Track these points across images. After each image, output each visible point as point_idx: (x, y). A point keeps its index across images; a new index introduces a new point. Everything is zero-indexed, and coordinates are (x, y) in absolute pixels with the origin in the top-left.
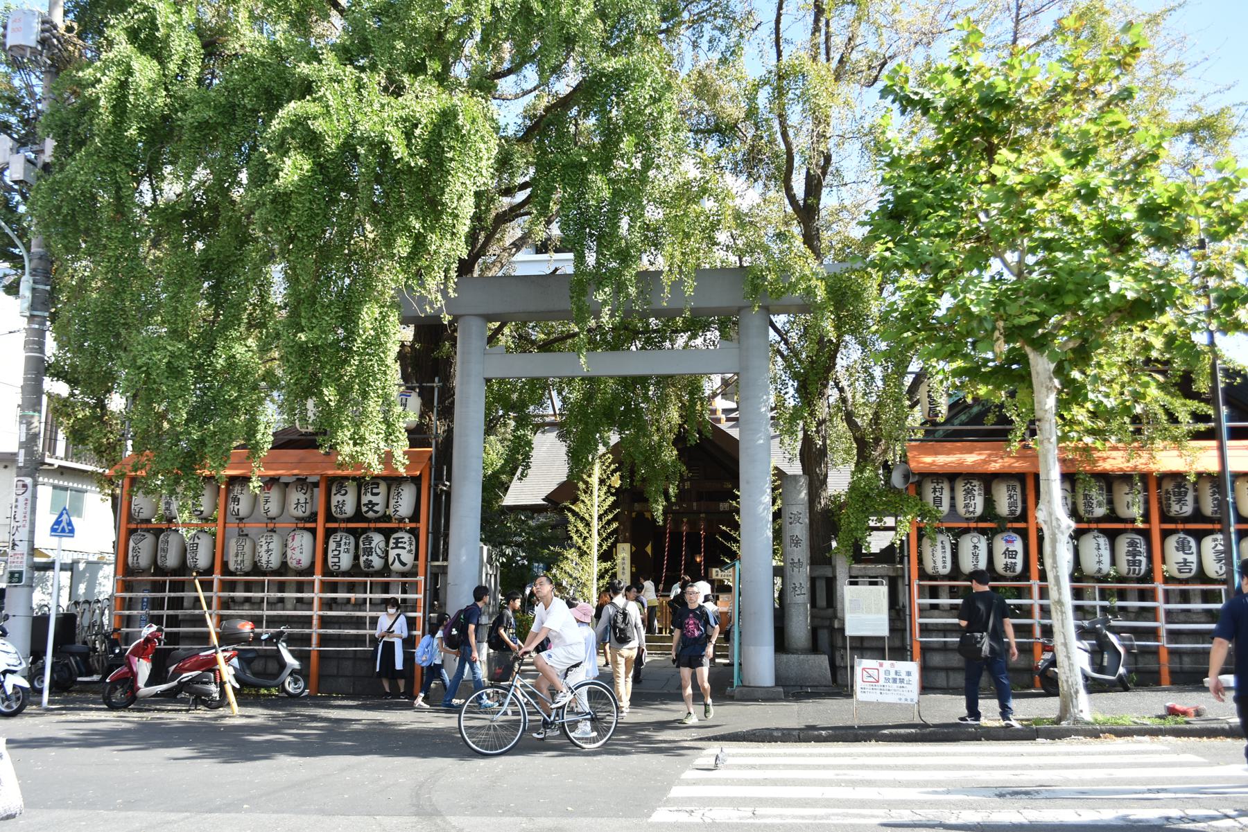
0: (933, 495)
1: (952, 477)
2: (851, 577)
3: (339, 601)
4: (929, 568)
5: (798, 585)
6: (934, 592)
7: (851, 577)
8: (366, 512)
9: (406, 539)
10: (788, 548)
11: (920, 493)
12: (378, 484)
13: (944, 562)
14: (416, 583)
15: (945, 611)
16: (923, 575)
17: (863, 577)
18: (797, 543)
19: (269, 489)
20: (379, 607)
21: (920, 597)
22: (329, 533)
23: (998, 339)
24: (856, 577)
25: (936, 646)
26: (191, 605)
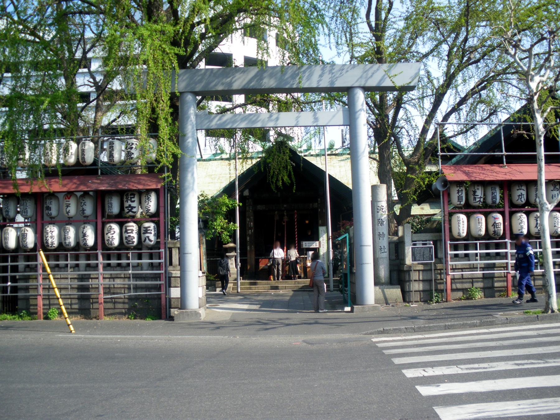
0: (458, 195)
1: (484, 184)
2: (413, 241)
3: (91, 265)
4: (455, 234)
5: (382, 247)
6: (455, 247)
7: (413, 241)
8: (128, 212)
9: (152, 228)
10: (377, 226)
11: (449, 195)
12: (134, 195)
13: (463, 230)
14: (160, 253)
15: (462, 258)
16: (452, 239)
17: (419, 241)
18: (251, 228)
19: (69, 199)
20: (115, 269)
21: (451, 251)
22: (512, 214)
23: (237, 29)
24: (416, 241)
25: (467, 270)
26: (23, 270)
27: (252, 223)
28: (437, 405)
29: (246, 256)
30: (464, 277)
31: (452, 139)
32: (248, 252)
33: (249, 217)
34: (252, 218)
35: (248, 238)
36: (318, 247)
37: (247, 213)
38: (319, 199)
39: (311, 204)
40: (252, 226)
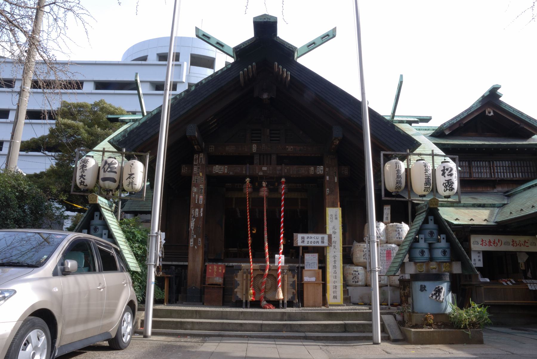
18: (198, 206)
27: (201, 197)
33: (197, 186)
34: (202, 186)
36: (326, 244)
37: (194, 178)
39: (312, 168)
40: (201, 202)
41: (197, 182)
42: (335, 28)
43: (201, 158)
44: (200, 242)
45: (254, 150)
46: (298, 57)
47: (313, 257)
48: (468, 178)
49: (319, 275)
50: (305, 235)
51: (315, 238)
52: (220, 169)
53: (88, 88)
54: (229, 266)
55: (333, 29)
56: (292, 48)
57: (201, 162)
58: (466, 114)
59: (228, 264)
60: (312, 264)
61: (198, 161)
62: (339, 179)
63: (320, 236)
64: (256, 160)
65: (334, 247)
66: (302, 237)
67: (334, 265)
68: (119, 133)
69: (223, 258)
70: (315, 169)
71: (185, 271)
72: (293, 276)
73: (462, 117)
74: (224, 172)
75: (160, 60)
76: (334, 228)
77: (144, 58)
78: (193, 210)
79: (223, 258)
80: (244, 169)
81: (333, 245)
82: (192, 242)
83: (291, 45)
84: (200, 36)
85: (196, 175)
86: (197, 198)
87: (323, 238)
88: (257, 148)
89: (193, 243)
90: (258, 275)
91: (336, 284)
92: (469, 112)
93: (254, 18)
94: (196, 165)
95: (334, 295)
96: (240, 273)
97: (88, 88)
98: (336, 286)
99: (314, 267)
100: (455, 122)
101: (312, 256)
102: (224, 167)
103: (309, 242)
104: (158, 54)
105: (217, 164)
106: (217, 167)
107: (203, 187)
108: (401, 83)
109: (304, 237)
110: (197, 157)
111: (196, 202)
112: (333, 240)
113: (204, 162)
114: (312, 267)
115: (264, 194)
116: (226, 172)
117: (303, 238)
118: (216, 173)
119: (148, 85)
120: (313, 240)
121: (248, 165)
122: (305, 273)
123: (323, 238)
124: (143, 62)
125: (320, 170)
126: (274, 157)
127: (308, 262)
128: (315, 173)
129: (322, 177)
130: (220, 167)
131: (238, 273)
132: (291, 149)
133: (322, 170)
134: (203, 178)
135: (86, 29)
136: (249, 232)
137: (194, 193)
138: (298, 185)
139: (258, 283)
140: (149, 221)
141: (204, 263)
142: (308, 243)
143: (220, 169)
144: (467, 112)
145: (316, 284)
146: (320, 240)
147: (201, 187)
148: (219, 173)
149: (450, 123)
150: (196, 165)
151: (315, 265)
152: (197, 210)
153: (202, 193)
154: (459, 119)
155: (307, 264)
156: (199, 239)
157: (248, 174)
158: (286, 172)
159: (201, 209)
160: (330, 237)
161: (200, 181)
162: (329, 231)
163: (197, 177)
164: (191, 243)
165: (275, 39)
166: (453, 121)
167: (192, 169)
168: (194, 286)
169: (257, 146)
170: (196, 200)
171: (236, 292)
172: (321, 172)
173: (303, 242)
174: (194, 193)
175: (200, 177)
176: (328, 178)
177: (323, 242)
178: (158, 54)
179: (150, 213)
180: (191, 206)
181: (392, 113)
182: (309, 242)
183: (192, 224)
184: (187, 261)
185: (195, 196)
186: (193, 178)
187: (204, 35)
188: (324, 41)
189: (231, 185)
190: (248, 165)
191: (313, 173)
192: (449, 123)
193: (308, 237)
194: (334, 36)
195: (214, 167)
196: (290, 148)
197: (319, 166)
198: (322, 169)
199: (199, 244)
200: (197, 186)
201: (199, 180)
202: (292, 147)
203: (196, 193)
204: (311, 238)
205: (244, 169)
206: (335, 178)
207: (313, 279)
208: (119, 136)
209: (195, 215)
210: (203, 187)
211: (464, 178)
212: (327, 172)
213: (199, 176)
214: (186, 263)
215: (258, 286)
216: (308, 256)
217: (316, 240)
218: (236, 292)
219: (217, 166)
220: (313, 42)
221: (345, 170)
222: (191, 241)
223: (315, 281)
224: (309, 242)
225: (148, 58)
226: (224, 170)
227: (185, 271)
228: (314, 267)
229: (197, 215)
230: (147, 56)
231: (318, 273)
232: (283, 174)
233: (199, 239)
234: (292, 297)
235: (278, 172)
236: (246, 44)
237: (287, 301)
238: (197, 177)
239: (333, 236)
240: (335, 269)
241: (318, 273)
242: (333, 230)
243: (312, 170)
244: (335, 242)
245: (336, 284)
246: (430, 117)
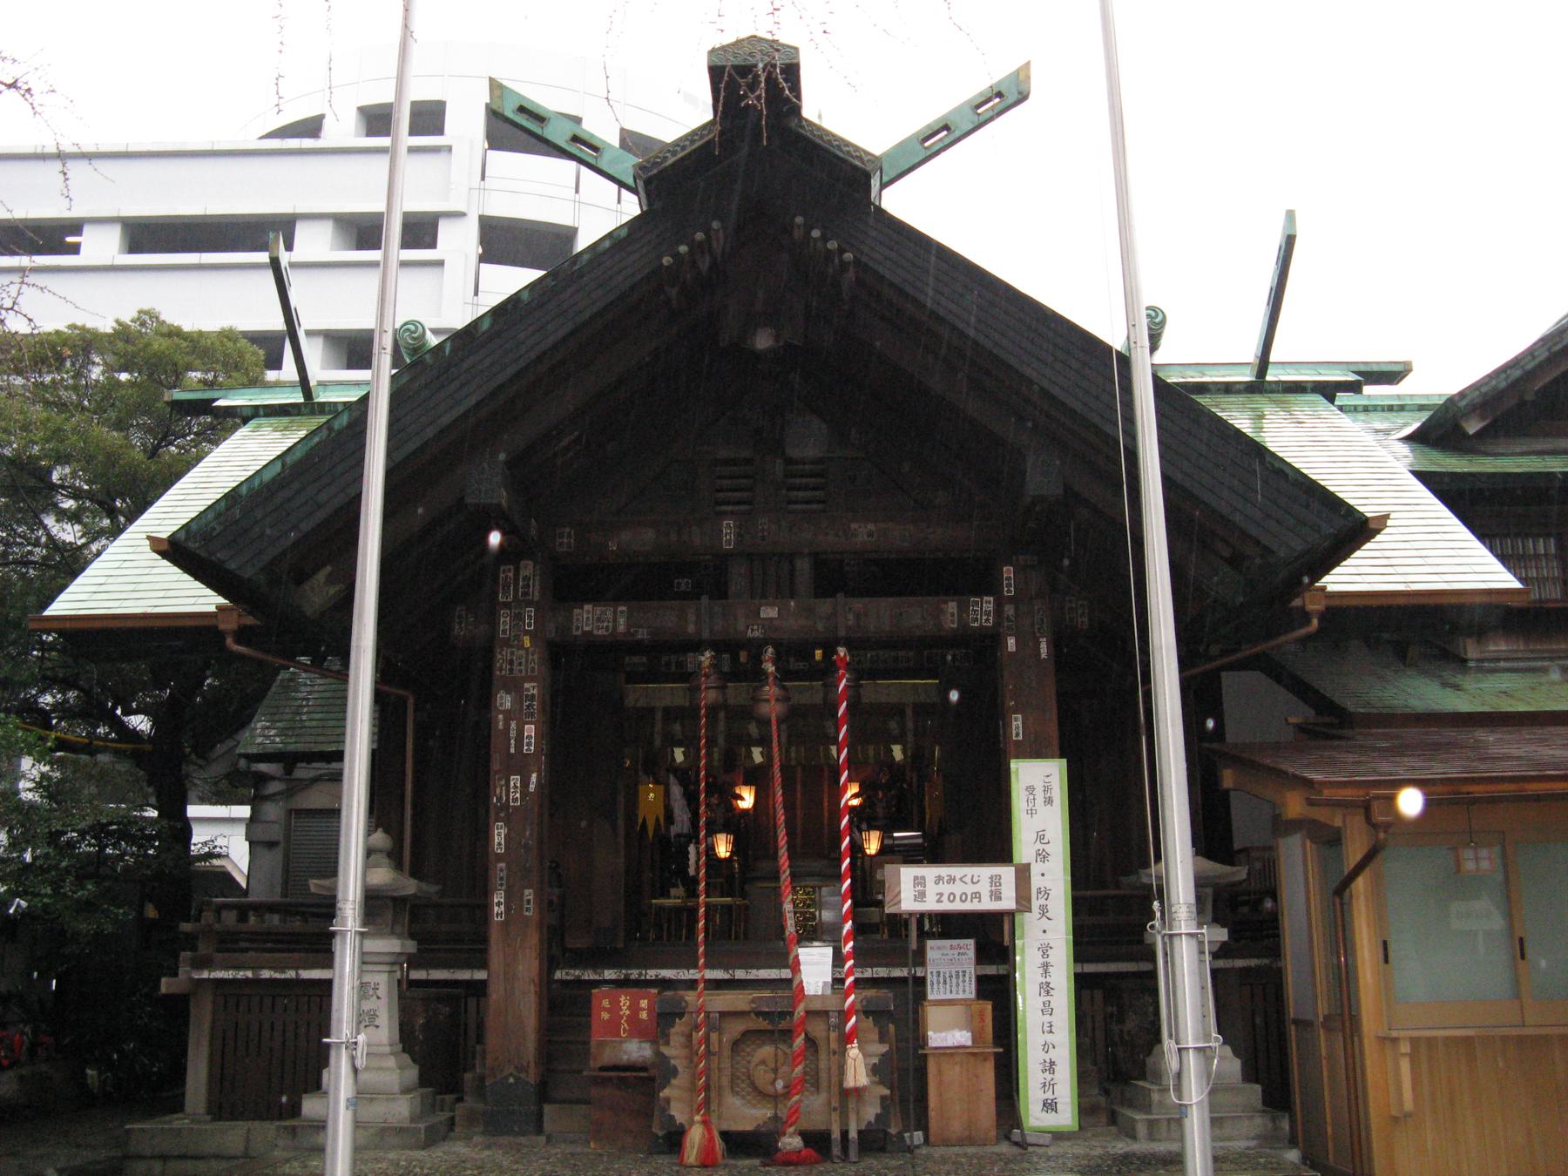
18: (520, 765)
27: (530, 730)
28: (572, 247)
29: (652, 710)
30: (384, 335)
31: (1204, 400)
32: (495, 936)
33: (514, 686)
34: (531, 688)
35: (499, 835)
36: (1008, 902)
37: (501, 656)
38: (1008, 571)
39: (952, 607)
40: (530, 748)
41: (511, 670)
42: (1028, 63)
43: (526, 578)
44: (529, 901)
45: (728, 542)
46: (884, 186)
47: (956, 952)
48: (1556, 601)
49: (983, 1020)
50: (930, 872)
51: (968, 879)
52: (599, 620)
53: (100, 246)
54: (646, 980)
55: (1018, 72)
56: (860, 158)
57: (526, 594)
58: (1543, 355)
59: (640, 974)
60: (954, 980)
61: (516, 591)
62: (1056, 645)
63: (984, 872)
64: (738, 577)
65: (1044, 911)
66: (916, 878)
67: (1044, 980)
68: (210, 507)
69: (620, 945)
70: (964, 608)
71: (478, 1001)
72: (880, 1033)
73: (1529, 367)
74: (615, 627)
75: (371, 132)
76: (1040, 837)
77: (311, 127)
78: (500, 779)
79: (620, 945)
80: (691, 618)
81: (1035, 904)
82: (499, 904)
83: (857, 149)
84: (509, 113)
85: (507, 643)
86: (513, 734)
87: (995, 881)
88: (739, 535)
89: (502, 907)
90: (748, 1031)
91: (1053, 1055)
92: (1555, 344)
93: (712, 52)
94: (506, 605)
95: (1046, 1096)
96: (673, 1104)
97: (100, 246)
98: (1052, 1063)
99: (961, 988)
100: (1503, 385)
101: (952, 947)
102: (615, 613)
103: (941, 894)
104: (363, 111)
105: (588, 601)
106: (588, 612)
107: (535, 692)
108: (1290, 241)
109: (923, 878)
110: (511, 575)
111: (512, 751)
112: (1036, 881)
113: (537, 594)
114: (954, 989)
115: (771, 712)
116: (622, 628)
117: (920, 881)
118: (585, 633)
119: (326, 230)
120: (958, 888)
121: (705, 600)
122: (933, 1015)
123: (995, 881)
124: (308, 143)
125: (983, 611)
126: (804, 566)
127: (938, 973)
128: (964, 625)
129: (992, 639)
130: (598, 610)
131: (673, 1027)
132: (870, 534)
133: (988, 613)
134: (536, 657)
135: (30, 320)
136: (703, 909)
137: (501, 717)
138: (902, 653)
139: (749, 1062)
140: (337, 778)
141: (550, 972)
142: (939, 901)
143: (599, 620)
144: (1548, 346)
145: (972, 1059)
146: (984, 888)
147: (528, 690)
148: (595, 632)
149: (1484, 390)
150: (506, 605)
151: (964, 981)
152: (515, 780)
153: (532, 715)
154: (1517, 373)
155: (935, 978)
156: (527, 892)
157: (706, 635)
158: (850, 623)
159: (530, 777)
160: (1023, 874)
161: (523, 668)
162: (1024, 846)
163: (512, 653)
164: (496, 909)
165: (793, 124)
166: (1494, 383)
167: (494, 624)
168: (511, 1074)
169: (740, 527)
170: (512, 742)
171: (668, 1100)
172: (987, 620)
173: (921, 896)
174: (501, 717)
175: (522, 652)
176: (1011, 643)
177: (996, 895)
178: (363, 111)
179: (339, 756)
180: (496, 765)
181: (1256, 357)
182: (945, 898)
183: (499, 835)
184: (484, 965)
185: (504, 725)
186: (499, 656)
187: (522, 109)
188: (982, 119)
189: (644, 659)
190: (705, 600)
191: (955, 626)
192: (1477, 389)
193: (939, 879)
194: (1023, 97)
195: (576, 611)
196: (863, 533)
197: (976, 595)
198: (991, 607)
199: (528, 909)
200: (514, 686)
201: (520, 664)
202: (871, 527)
203: (509, 716)
204: (952, 880)
205: (691, 618)
206: (1039, 643)
207: (961, 1037)
208: (211, 516)
209: (508, 799)
210: (535, 692)
211: (1540, 601)
212: (1008, 619)
213: (521, 647)
214: (480, 975)
215: (749, 1077)
216: (939, 948)
217: (970, 889)
218: (668, 1100)
219: (588, 607)
220: (941, 125)
221: (1080, 611)
222: (496, 900)
223: (969, 1043)
224: (941, 894)
225: (326, 124)
226: (615, 620)
227: (478, 1001)
228: (961, 988)
229: (515, 800)
230: (321, 118)
231: (982, 1014)
232: (842, 633)
233: (527, 892)
234: (878, 1116)
235: (820, 626)
236: (683, 148)
237: (860, 1132)
238: (512, 653)
239: (1035, 870)
240: (1048, 998)
241: (982, 1014)
242: (1039, 846)
243: (952, 615)
244: (1046, 893)
245: (1053, 1055)
246: (1404, 363)
